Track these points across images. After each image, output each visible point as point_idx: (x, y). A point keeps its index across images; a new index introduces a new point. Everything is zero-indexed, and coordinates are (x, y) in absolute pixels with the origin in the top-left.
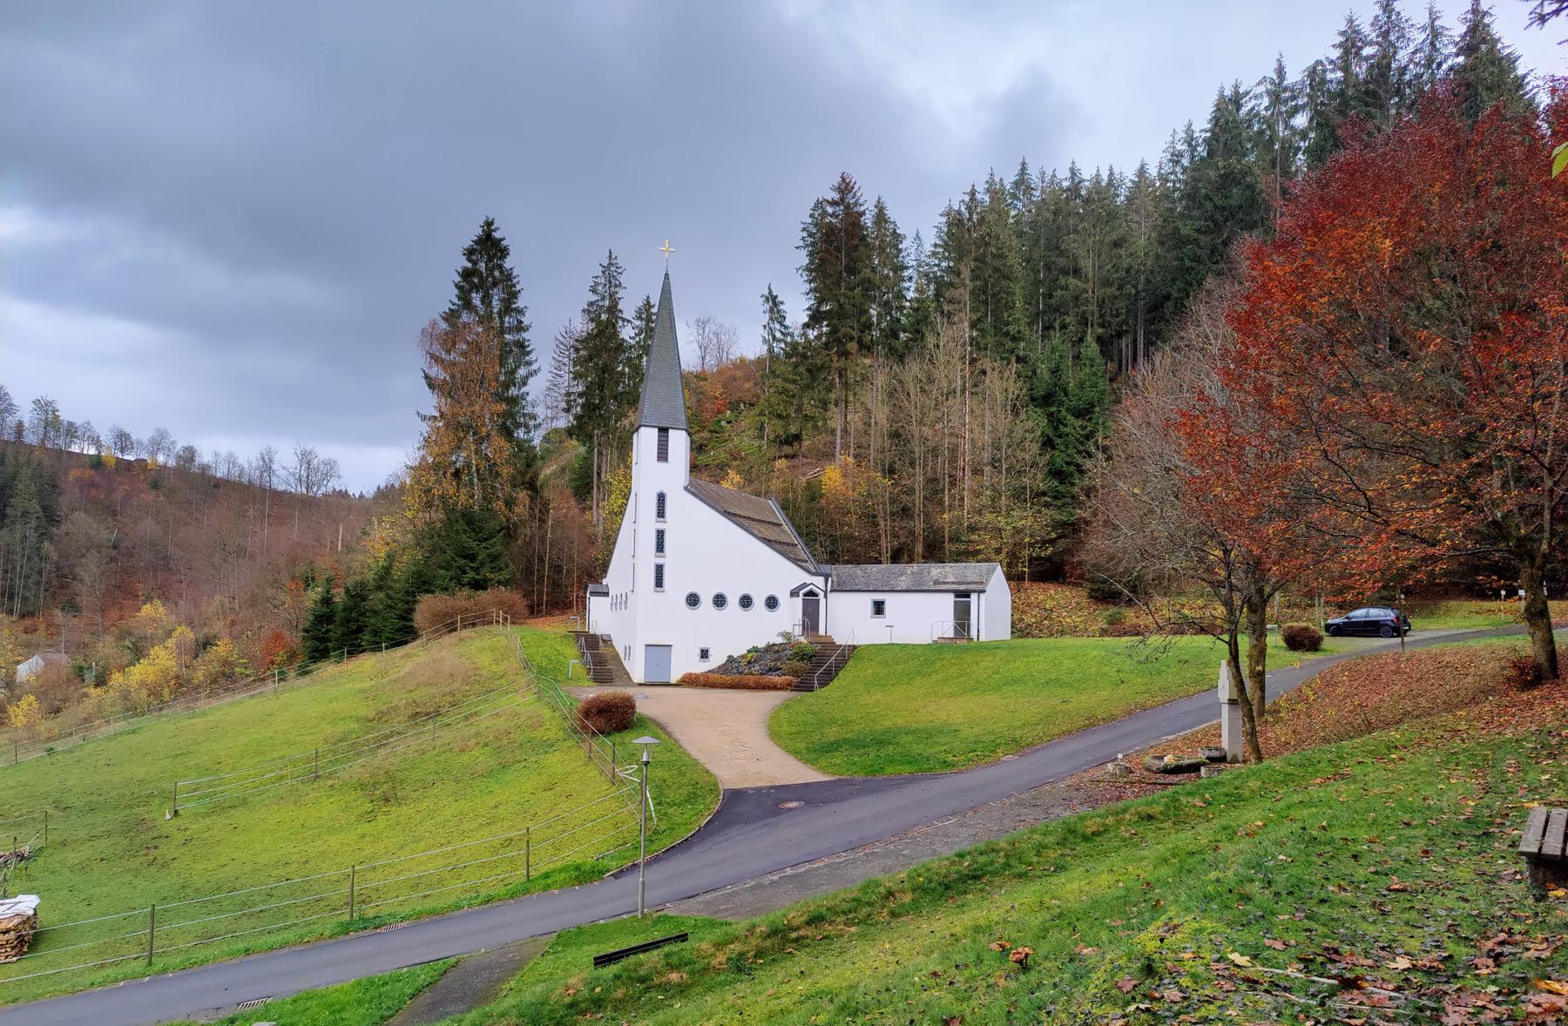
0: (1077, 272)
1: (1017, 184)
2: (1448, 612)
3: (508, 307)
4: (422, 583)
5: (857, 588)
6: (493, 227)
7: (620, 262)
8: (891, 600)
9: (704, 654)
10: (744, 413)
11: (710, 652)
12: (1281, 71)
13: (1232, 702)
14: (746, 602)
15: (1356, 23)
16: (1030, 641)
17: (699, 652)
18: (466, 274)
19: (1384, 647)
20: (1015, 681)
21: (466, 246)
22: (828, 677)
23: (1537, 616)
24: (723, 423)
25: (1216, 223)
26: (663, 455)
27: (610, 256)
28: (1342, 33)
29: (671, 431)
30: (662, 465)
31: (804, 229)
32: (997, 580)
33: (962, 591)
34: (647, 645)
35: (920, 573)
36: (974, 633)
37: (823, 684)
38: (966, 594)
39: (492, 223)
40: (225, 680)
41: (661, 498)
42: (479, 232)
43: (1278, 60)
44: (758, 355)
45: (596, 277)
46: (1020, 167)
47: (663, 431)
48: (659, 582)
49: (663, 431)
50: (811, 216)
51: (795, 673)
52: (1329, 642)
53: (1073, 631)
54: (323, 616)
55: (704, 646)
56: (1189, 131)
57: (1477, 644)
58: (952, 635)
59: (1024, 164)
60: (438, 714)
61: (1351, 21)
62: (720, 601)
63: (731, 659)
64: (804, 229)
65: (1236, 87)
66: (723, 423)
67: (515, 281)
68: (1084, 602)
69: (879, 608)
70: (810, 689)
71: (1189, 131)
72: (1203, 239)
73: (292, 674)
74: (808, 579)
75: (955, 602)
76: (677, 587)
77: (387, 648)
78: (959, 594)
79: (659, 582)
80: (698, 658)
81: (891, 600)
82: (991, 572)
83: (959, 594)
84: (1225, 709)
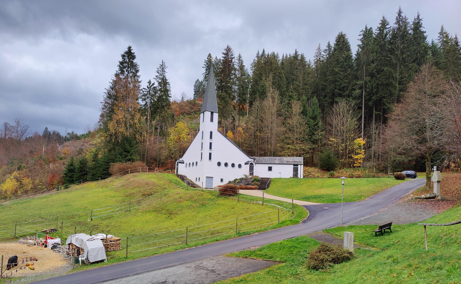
3: (135, 75)
4: (109, 161)
5: (263, 163)
6: (131, 49)
7: (166, 64)
8: (274, 167)
9: (222, 180)
11: (223, 180)
14: (226, 165)
15: (385, 18)
17: (220, 180)
18: (121, 63)
21: (122, 54)
26: (212, 120)
27: (163, 62)
28: (382, 21)
29: (214, 113)
30: (212, 123)
31: (205, 62)
33: (296, 164)
34: (206, 177)
37: (268, 188)
38: (297, 165)
39: (131, 47)
40: (36, 190)
41: (211, 133)
42: (127, 50)
43: (366, 26)
44: (187, 99)
45: (158, 68)
46: (263, 51)
48: (210, 158)
49: (212, 113)
50: (208, 58)
51: (257, 185)
54: (71, 169)
55: (222, 178)
58: (292, 177)
59: (264, 50)
60: (152, 194)
61: (384, 17)
62: (233, 165)
63: (230, 182)
64: (205, 62)
67: (138, 67)
69: (270, 169)
72: (342, 73)
73: (63, 188)
74: (250, 160)
75: (294, 167)
76: (215, 159)
77: (101, 179)
78: (294, 165)
79: (210, 158)
80: (220, 181)
81: (274, 167)
83: (294, 165)
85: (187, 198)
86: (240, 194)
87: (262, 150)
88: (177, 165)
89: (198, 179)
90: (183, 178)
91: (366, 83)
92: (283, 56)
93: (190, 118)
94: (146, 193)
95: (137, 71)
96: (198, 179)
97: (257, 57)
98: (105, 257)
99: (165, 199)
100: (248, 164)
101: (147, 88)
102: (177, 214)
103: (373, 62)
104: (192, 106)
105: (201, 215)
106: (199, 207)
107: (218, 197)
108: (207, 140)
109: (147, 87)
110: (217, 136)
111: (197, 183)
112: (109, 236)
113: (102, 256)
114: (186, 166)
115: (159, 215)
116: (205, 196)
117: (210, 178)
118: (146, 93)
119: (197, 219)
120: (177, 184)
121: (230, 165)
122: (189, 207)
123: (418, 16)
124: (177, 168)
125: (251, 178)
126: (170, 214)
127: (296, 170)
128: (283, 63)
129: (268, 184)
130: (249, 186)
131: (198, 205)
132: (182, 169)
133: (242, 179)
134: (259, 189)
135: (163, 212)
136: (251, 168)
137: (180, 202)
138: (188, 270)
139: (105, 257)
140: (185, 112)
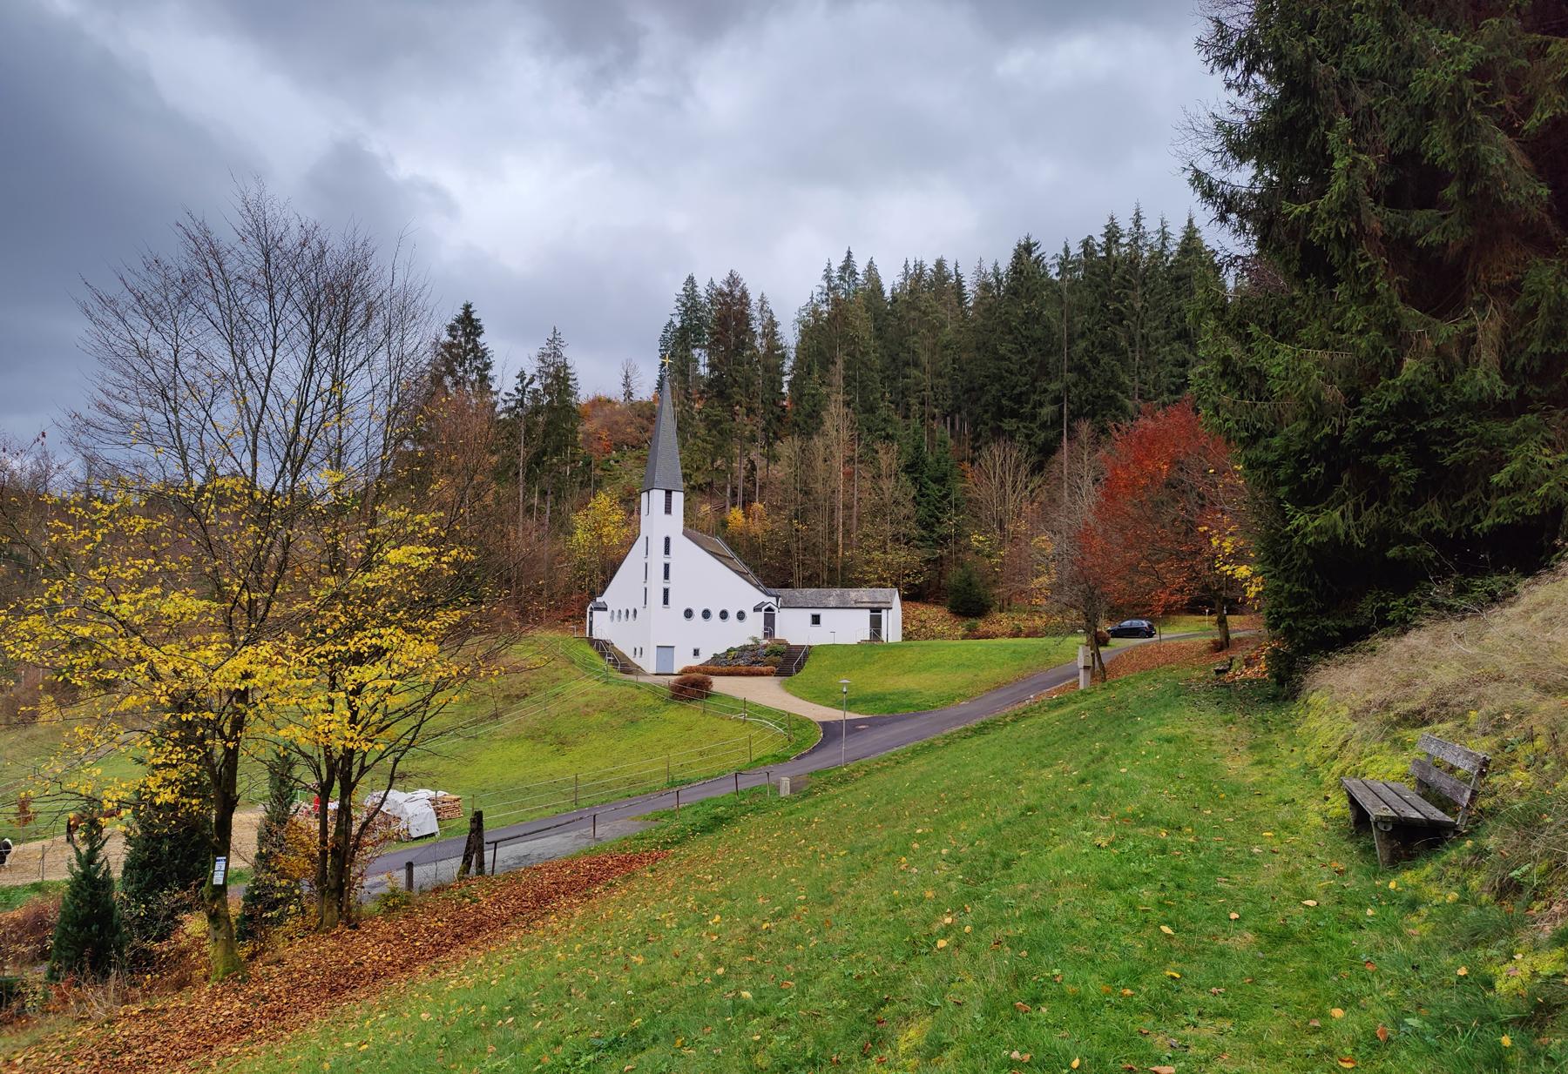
0: (916, 365)
1: (843, 269)
2: (1174, 623)
8: (824, 614)
9: (696, 653)
10: (628, 454)
12: (1067, 250)
13: (1086, 668)
14: (706, 614)
16: (912, 642)
19: (1135, 647)
20: (936, 666)
22: (800, 667)
23: (1222, 622)
24: (612, 462)
25: (1023, 348)
26: (668, 510)
28: (1107, 227)
32: (897, 602)
35: (842, 595)
36: (884, 637)
37: (797, 672)
38: (879, 610)
41: (667, 540)
42: (461, 313)
47: (669, 493)
48: (666, 602)
49: (669, 493)
50: (684, 289)
51: (774, 664)
52: (1113, 641)
53: (942, 636)
56: (996, 268)
57: (1197, 639)
59: (849, 252)
61: (1112, 219)
63: (716, 656)
65: (1028, 238)
66: (612, 462)
68: (948, 616)
69: (816, 620)
70: (789, 674)
71: (996, 268)
72: (1014, 358)
74: (766, 599)
76: (678, 603)
78: (873, 610)
79: (666, 602)
81: (824, 614)
82: (892, 595)
83: (873, 610)
84: (1082, 672)
85: (602, 706)
86: (715, 695)
87: (1460, 109)
88: (591, 613)
89: (638, 651)
90: (603, 647)
91: (1068, 389)
92: (906, 266)
93: (638, 458)
94: (513, 692)
95: (488, 366)
96: (638, 651)
97: (828, 278)
98: (436, 829)
99: (555, 708)
100: (760, 610)
101: (515, 392)
102: (575, 743)
103: (1082, 335)
104: (645, 422)
105: (623, 745)
106: (624, 727)
107: (667, 702)
108: (657, 559)
109: (517, 389)
110: (681, 544)
111: (637, 661)
112: (441, 793)
113: (432, 826)
114: (612, 618)
115: (539, 746)
116: (640, 702)
117: (666, 650)
118: (512, 404)
119: (615, 754)
120: (588, 667)
121: (715, 614)
122: (602, 728)
123: (1190, 221)
124: (591, 622)
125: (765, 646)
126: (562, 743)
127: (876, 624)
128: (895, 300)
129: (799, 663)
130: (757, 668)
131: (622, 721)
132: (602, 626)
133: (744, 649)
134: (778, 674)
135: (548, 738)
136: (769, 621)
137: (587, 714)
138: (566, 840)
139: (436, 829)
140: (624, 442)
